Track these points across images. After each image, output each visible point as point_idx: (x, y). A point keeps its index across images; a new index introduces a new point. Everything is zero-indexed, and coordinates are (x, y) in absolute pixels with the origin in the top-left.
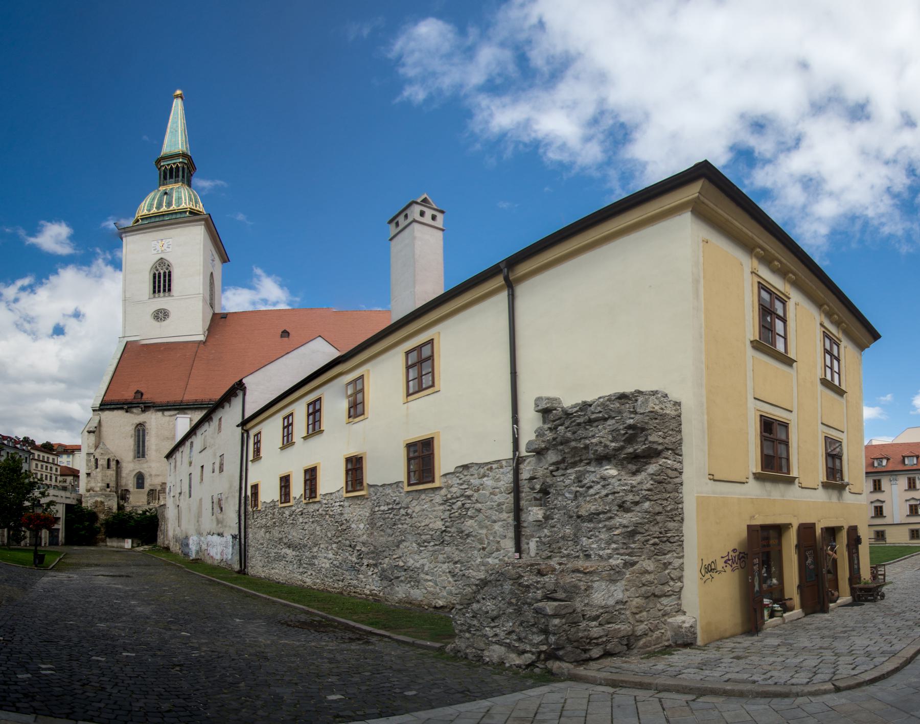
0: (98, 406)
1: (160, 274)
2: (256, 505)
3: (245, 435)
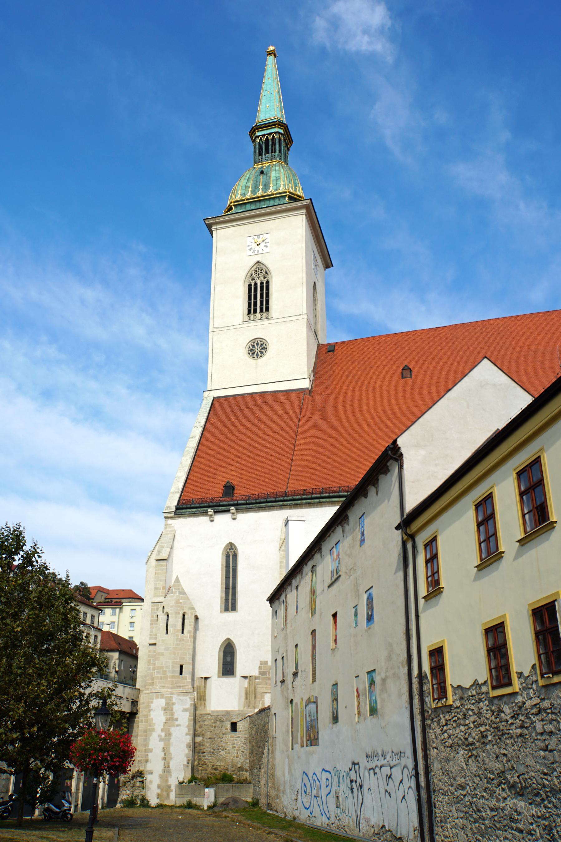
0: (174, 510)
1: (256, 284)
2: (442, 692)
3: (409, 546)
